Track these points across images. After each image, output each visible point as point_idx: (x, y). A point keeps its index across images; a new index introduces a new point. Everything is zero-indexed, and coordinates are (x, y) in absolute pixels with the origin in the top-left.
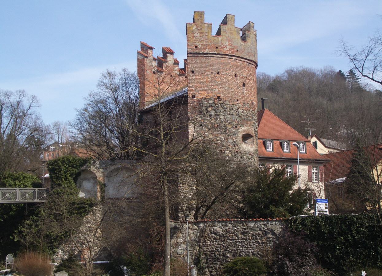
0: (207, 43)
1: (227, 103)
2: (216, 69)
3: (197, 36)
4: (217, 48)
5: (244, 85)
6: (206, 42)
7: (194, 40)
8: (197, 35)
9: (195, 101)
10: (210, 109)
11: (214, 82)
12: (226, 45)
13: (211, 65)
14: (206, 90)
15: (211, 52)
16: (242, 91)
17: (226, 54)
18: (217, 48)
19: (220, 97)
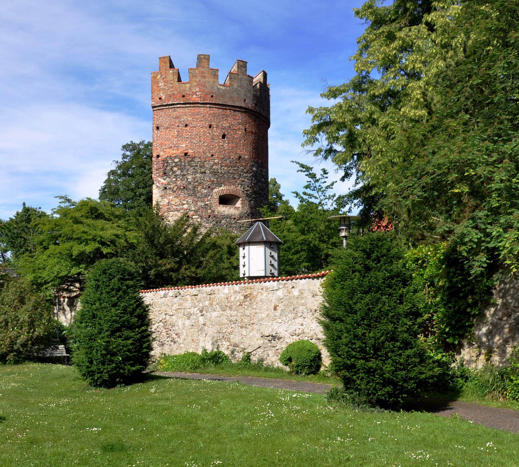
2: (184, 121)
4: (184, 96)
5: (224, 137)
10: (175, 169)
13: (177, 117)
14: (171, 147)
15: (176, 103)
16: (221, 144)
18: (184, 96)
19: (187, 153)
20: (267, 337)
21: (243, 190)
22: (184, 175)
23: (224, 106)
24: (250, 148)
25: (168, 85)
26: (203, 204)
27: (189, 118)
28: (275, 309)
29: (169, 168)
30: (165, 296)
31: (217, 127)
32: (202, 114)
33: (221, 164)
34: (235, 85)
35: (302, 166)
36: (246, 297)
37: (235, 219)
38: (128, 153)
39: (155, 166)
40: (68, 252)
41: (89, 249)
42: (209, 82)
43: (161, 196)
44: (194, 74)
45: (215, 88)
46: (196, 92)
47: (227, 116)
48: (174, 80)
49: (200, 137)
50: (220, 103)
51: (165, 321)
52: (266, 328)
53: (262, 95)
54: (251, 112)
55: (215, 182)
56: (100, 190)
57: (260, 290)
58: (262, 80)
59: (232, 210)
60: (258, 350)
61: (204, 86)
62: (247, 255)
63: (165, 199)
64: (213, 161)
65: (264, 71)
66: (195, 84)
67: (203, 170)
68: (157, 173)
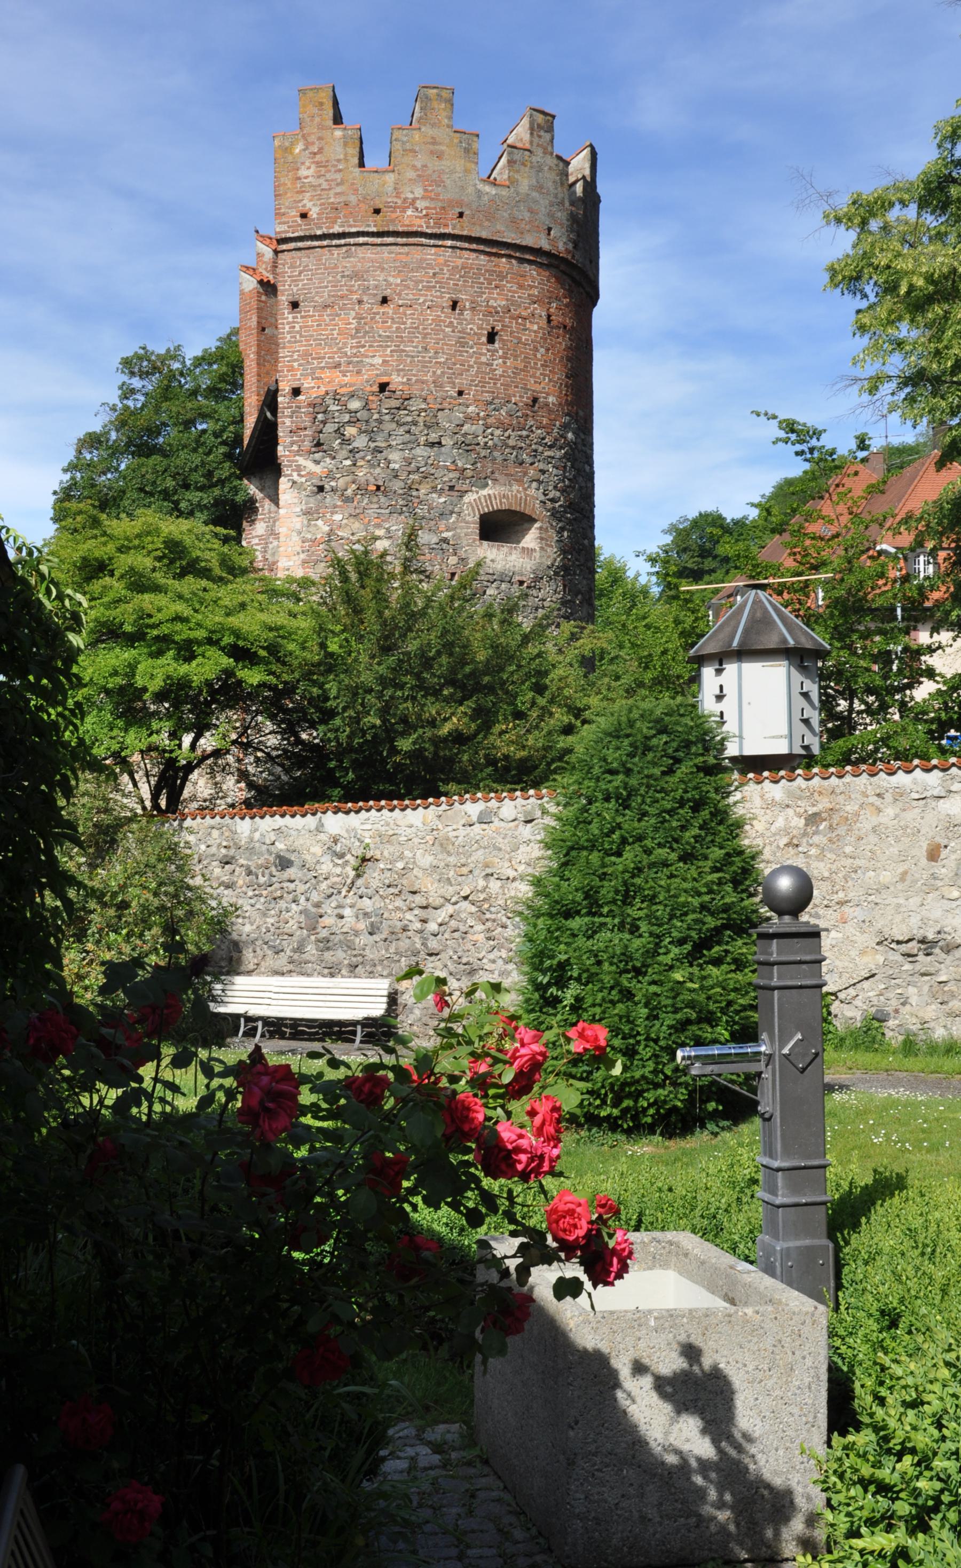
0: (342, 199)
1: (415, 405)
2: (376, 287)
3: (306, 177)
4: (377, 211)
5: (491, 337)
6: (337, 194)
7: (298, 192)
8: (307, 172)
9: (299, 407)
10: (350, 431)
11: (367, 332)
12: (414, 200)
13: (356, 275)
14: (338, 365)
15: (354, 230)
16: (484, 359)
17: (415, 229)
18: (377, 211)
19: (387, 384)
20: (899, 942)
21: (542, 498)
22: (378, 450)
23: (492, 246)
24: (560, 375)
25: (328, 176)
26: (435, 539)
27: (391, 279)
28: (933, 854)
29: (330, 428)
30: (484, 820)
31: (473, 309)
32: (430, 266)
33: (484, 419)
34: (525, 184)
35: (790, 426)
36: (813, 819)
37: (521, 583)
38: (136, 383)
39: (288, 422)
40: (120, 681)
41: (206, 668)
42: (452, 172)
43: (307, 513)
44: (408, 146)
45: (470, 190)
46: (414, 200)
47: (501, 277)
48: (346, 160)
49: (425, 336)
50: (484, 235)
51: (482, 896)
52: (898, 918)
53: (584, 215)
54: (562, 267)
55: (469, 473)
56: (55, 493)
57: (873, 799)
58: (587, 172)
59: (514, 557)
60: (866, 984)
61: (439, 183)
62: (729, 690)
63: (320, 523)
64: (462, 408)
65: (591, 146)
66: (411, 174)
67: (433, 437)
68: (292, 443)
